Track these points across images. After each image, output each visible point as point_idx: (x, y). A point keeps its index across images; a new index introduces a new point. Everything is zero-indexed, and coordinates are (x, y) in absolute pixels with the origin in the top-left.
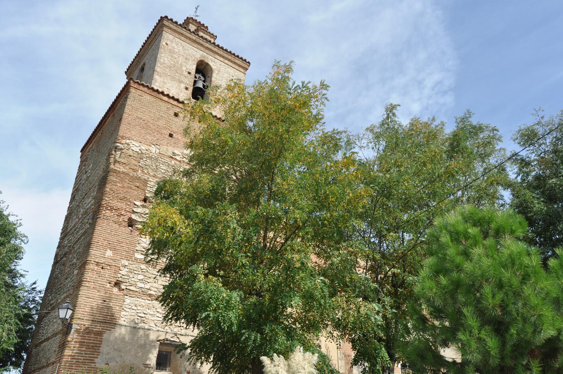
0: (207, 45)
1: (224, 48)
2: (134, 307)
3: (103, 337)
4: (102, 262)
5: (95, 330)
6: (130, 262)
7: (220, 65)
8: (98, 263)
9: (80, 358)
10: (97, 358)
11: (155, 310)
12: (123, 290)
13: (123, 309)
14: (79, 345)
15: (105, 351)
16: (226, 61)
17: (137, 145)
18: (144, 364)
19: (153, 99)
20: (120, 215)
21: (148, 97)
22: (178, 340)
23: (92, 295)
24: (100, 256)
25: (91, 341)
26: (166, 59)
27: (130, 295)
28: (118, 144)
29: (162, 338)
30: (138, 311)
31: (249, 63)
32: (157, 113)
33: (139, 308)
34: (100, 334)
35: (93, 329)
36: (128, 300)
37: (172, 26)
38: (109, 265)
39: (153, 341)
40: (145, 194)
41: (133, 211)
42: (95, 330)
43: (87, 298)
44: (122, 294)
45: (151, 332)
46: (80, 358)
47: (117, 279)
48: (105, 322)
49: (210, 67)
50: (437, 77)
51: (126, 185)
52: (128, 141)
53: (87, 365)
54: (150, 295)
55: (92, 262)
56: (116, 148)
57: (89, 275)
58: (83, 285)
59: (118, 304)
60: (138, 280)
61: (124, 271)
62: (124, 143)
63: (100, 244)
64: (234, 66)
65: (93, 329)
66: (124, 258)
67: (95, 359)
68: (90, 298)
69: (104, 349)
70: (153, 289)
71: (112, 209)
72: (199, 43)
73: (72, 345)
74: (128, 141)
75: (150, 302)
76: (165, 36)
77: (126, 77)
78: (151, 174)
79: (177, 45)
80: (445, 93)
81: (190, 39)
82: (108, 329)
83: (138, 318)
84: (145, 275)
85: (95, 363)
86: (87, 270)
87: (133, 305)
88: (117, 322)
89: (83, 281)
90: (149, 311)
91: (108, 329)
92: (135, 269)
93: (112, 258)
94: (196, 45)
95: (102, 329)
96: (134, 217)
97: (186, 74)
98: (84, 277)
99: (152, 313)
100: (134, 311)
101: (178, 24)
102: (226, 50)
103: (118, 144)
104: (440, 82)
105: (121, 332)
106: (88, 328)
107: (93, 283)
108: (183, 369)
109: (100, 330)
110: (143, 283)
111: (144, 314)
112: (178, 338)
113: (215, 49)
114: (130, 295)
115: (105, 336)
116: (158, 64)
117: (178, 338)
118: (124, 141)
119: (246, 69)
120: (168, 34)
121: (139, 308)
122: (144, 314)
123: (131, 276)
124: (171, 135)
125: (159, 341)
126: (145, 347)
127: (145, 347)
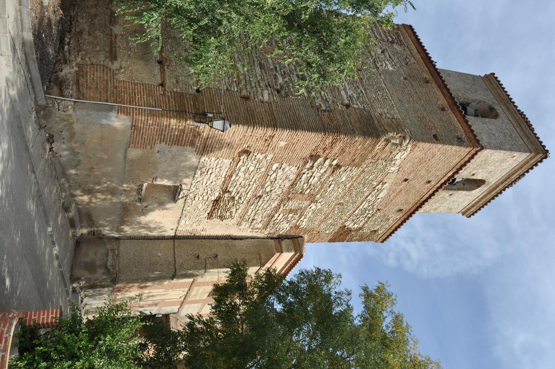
0: (501, 187)
1: (492, 200)
2: (219, 166)
3: (188, 147)
4: (273, 140)
5: (197, 140)
6: (269, 161)
7: (475, 196)
8: (273, 137)
9: (167, 132)
10: (166, 144)
11: (214, 180)
12: (240, 156)
13: (218, 158)
14: (182, 129)
15: (173, 149)
16: (477, 200)
17: (402, 157)
18: (156, 177)
19: (452, 165)
20: (324, 150)
21: (455, 162)
22: (180, 197)
23: (237, 136)
24: (280, 138)
25: (184, 138)
26: (496, 157)
27: (232, 163)
28: (408, 141)
29: (184, 187)
30: (214, 169)
31: (470, 217)
32: (435, 169)
33: (218, 170)
34: (192, 144)
35: (198, 139)
36: (227, 162)
37: (534, 160)
38: (268, 146)
39: (181, 181)
40: (344, 166)
41: (327, 159)
42: (197, 140)
43: (234, 132)
44: (235, 155)
45: (191, 180)
46: (167, 132)
47: (252, 152)
48: (205, 148)
49: (475, 189)
50: (415, 255)
51: (358, 152)
52: (409, 149)
53: (159, 137)
54: (231, 176)
55: (275, 133)
56: (404, 138)
57: (260, 132)
58: (250, 127)
59: (224, 155)
60: (248, 167)
61: (260, 156)
62: (408, 147)
63: (295, 137)
64: (470, 205)
65: (198, 139)
66: (275, 156)
67: (164, 143)
68: (233, 134)
69: (175, 148)
70: (237, 178)
71: (333, 143)
72: (506, 180)
73: (182, 124)
74: (409, 149)
75: (223, 176)
76: (524, 155)
77: (488, 74)
78: (366, 169)
79: (510, 164)
80: (398, 259)
81: (513, 174)
82: (198, 150)
83: (207, 170)
84: (254, 171)
85: (160, 143)
86: (266, 129)
87: (222, 165)
88: (204, 155)
89: (254, 127)
90: (214, 176)
91: (198, 150)
92: (261, 164)
93: (277, 147)
94: (504, 178)
95: (197, 146)
96: (320, 160)
97: (474, 172)
98: (258, 128)
99: (211, 178)
100: (215, 166)
101: (534, 167)
102: (489, 201)
103: (408, 141)
104: (409, 257)
105: (193, 159)
106: (200, 135)
107: (250, 134)
108: (150, 202)
109: (197, 144)
110: (245, 171)
111: (211, 174)
112: (182, 198)
113: (494, 193)
114: (232, 163)
115: (189, 148)
116: (492, 151)
117: (182, 198)
118: (410, 146)
119: (463, 214)
120: (526, 157)
121: (218, 170)
122: (211, 174)
123: (254, 162)
124: (406, 180)
125: (181, 185)
126: (175, 175)
127: (175, 175)
